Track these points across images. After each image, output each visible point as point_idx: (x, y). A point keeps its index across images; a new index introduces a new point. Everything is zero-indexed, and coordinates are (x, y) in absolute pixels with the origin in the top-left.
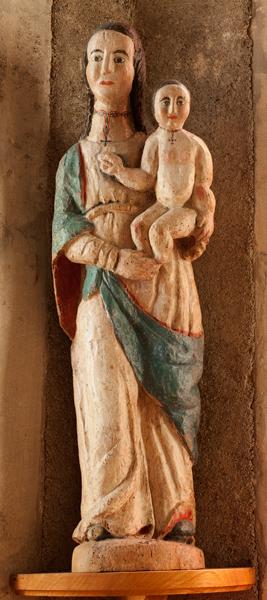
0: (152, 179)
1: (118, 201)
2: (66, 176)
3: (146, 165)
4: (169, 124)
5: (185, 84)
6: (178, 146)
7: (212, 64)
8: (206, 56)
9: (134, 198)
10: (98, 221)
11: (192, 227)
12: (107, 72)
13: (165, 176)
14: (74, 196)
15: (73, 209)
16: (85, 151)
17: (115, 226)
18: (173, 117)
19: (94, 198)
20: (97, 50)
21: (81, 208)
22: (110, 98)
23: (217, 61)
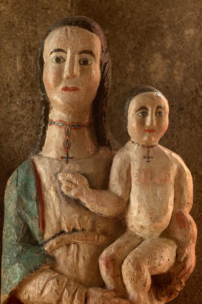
0: (125, 203)
1: (83, 230)
2: (19, 200)
4: (146, 138)
7: (172, 66)
8: (165, 56)
9: (101, 225)
10: (60, 253)
11: (172, 261)
12: (72, 76)
13: (140, 200)
14: (30, 223)
15: (29, 240)
16: (41, 169)
17: (81, 260)
18: (151, 131)
20: (84, 52)
21: (38, 238)
22: (72, 107)
23: (178, 63)
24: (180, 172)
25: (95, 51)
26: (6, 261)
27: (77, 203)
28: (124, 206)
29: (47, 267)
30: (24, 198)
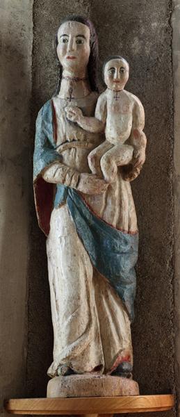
0: (103, 125)
1: (79, 140)
4: (114, 86)
7: (144, 44)
8: (140, 39)
9: (90, 137)
10: (65, 154)
11: (130, 158)
12: (72, 50)
13: (111, 122)
14: (49, 136)
15: (48, 145)
16: (56, 105)
17: (77, 157)
18: (117, 82)
20: (65, 35)
21: (53, 145)
22: (73, 68)
24: (136, 106)
25: (86, 36)
26: (35, 157)
27: (75, 124)
28: (103, 126)
29: (58, 161)
30: (45, 122)
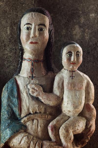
0: (60, 100)
1: (40, 113)
2: (9, 98)
3: (56, 91)
4: (71, 67)
5: (78, 43)
6: (76, 80)
7: (84, 32)
8: (80, 27)
9: (49, 110)
10: (29, 124)
11: (84, 127)
12: (35, 36)
13: (68, 98)
14: (14, 109)
16: (19, 82)
17: (39, 127)
18: (74, 63)
19: (26, 111)
21: (18, 116)
22: (35, 52)
23: (87, 30)
